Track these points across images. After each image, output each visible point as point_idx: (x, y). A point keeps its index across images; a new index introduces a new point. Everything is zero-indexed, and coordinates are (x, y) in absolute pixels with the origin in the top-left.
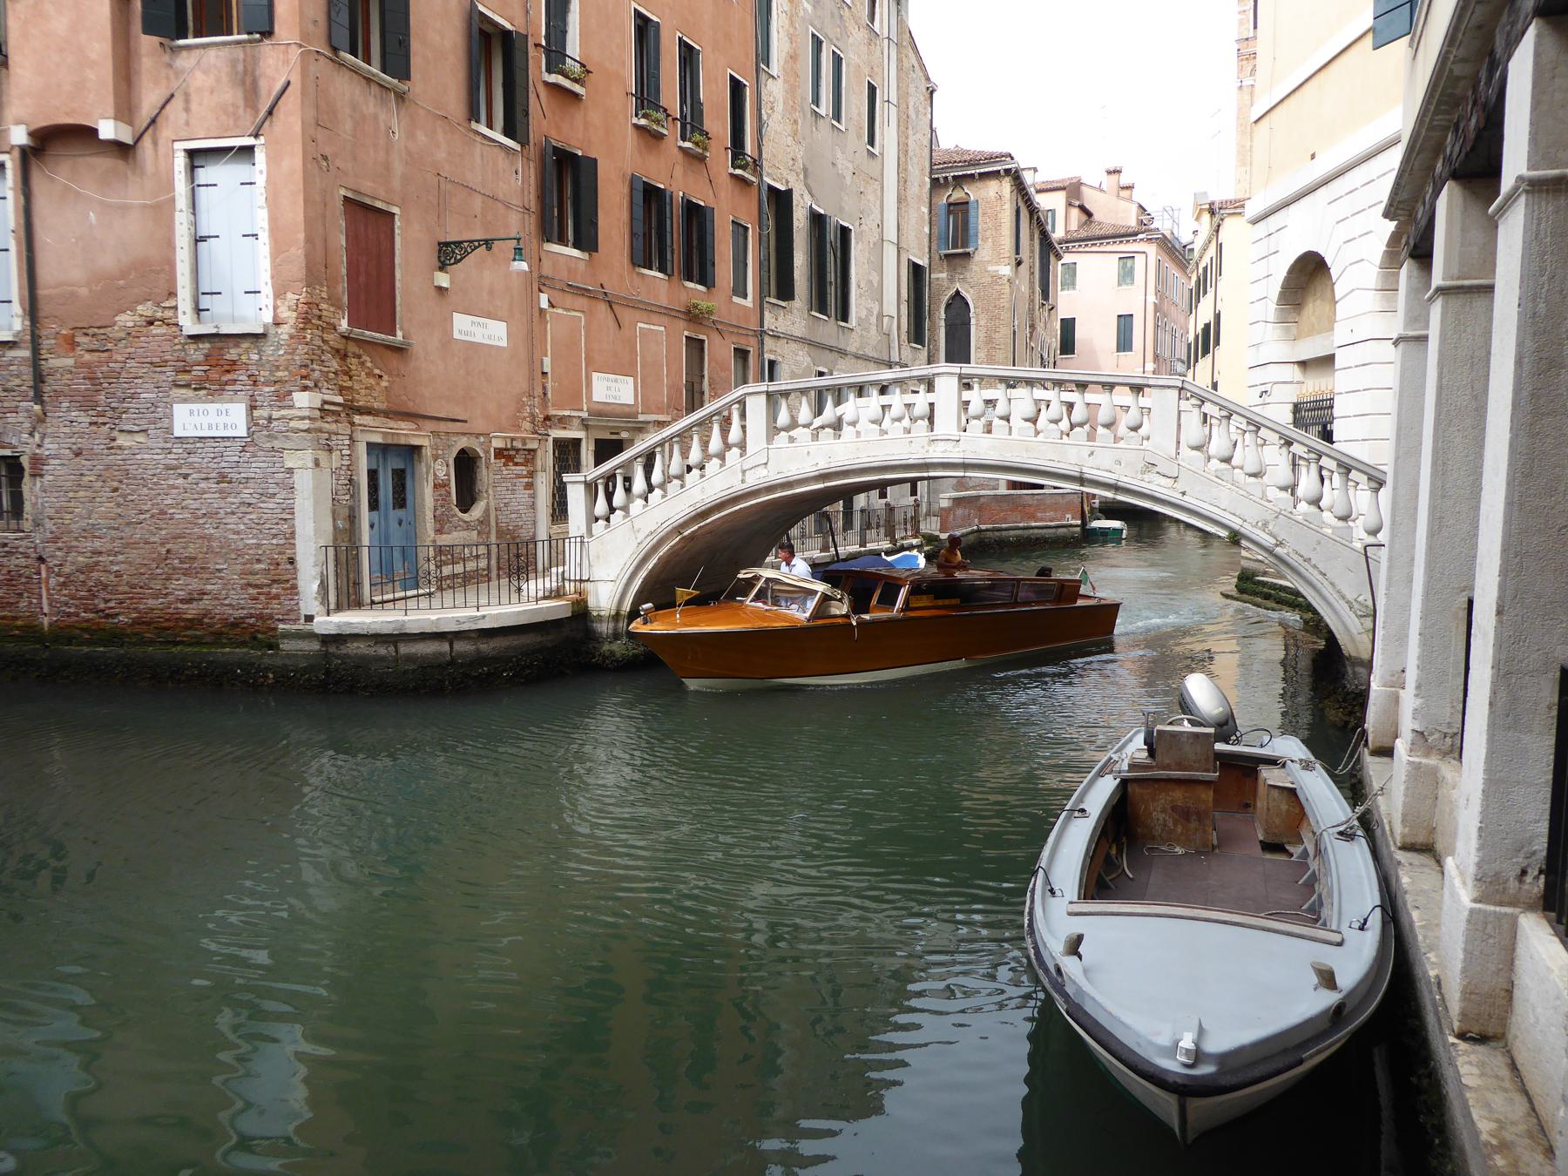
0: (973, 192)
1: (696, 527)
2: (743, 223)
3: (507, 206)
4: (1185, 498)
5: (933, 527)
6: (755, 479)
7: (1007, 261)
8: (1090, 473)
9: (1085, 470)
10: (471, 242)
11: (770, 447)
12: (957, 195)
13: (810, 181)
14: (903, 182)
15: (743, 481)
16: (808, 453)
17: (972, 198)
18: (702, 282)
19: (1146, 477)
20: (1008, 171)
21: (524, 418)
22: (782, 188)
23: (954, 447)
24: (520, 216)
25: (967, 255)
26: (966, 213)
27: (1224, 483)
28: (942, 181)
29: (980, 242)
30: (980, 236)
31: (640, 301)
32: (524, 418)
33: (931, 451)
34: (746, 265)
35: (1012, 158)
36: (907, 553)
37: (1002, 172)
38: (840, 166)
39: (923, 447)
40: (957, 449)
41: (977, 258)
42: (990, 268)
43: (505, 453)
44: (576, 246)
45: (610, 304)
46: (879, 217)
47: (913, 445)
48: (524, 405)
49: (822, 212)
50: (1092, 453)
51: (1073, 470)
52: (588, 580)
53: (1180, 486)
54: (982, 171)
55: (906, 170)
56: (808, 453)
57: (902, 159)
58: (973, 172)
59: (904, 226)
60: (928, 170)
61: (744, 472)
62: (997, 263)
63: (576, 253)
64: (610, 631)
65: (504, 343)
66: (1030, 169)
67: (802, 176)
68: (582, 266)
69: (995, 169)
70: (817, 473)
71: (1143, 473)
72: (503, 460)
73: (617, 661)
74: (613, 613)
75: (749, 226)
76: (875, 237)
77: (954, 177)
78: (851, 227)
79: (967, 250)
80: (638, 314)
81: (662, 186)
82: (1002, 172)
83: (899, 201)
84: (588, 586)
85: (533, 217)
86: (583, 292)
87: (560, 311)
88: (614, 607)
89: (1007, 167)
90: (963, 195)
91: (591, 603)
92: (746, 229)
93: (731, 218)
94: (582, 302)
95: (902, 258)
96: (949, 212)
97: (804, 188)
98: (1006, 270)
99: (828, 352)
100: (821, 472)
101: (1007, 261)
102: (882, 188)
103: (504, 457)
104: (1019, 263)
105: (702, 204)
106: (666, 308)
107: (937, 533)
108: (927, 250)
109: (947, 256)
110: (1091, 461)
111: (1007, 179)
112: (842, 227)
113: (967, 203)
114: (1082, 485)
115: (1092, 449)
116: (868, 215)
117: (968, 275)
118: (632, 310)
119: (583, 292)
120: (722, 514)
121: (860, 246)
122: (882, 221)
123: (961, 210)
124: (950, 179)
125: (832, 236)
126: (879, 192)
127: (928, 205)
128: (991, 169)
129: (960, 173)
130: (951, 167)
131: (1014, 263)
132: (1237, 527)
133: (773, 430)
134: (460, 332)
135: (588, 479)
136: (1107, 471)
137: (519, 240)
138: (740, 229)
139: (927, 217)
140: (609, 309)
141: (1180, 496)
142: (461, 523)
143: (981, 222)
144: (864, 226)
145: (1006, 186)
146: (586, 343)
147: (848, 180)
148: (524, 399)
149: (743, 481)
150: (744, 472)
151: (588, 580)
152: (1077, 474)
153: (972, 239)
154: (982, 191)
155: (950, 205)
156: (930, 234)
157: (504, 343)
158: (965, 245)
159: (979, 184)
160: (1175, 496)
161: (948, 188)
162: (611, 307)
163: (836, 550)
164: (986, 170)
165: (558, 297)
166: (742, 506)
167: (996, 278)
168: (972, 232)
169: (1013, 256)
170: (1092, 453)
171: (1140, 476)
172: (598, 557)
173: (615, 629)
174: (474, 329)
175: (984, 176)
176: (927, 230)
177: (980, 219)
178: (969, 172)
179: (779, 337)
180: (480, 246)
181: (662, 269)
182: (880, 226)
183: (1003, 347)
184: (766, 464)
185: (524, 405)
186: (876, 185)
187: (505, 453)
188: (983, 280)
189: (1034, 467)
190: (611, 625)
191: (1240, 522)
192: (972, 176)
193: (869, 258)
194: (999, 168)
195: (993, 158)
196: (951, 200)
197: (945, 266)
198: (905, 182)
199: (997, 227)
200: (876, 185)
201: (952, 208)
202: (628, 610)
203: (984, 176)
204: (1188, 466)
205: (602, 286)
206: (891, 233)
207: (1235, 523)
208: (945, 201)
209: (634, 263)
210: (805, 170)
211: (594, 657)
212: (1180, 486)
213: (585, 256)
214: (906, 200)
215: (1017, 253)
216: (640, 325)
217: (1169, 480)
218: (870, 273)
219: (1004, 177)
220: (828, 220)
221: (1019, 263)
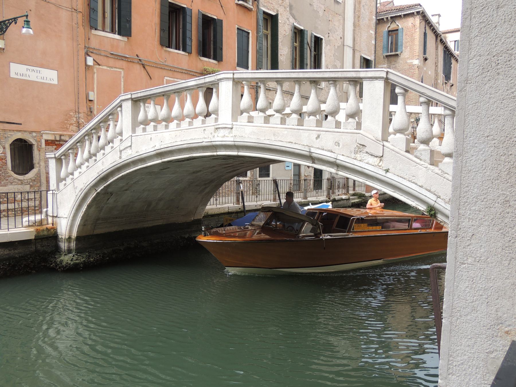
0: (400, 24)
1: (103, 187)
2: (245, 30)
3: (59, 6)
4: (389, 175)
5: (363, 190)
6: (128, 155)
7: (417, 57)
8: (317, 152)
9: (313, 150)
10: (9, 20)
11: (133, 135)
12: (393, 26)
13: (294, 12)
14: (357, 17)
15: (120, 158)
16: (151, 139)
17: (400, 27)
18: (215, 59)
19: (358, 156)
20: (418, 13)
21: (72, 124)
22: (273, 13)
23: (229, 133)
24: (70, 13)
25: (397, 55)
26: (397, 35)
27: (422, 163)
28: (385, 20)
29: (403, 48)
30: (404, 46)
31: (167, 65)
32: (72, 124)
33: (216, 136)
34: (248, 52)
35: (421, 6)
36: (325, 204)
37: (415, 13)
38: (315, 6)
39: (211, 133)
40: (231, 135)
41: (402, 56)
42: (409, 61)
43: (57, 143)
44: (119, 34)
45: (144, 66)
46: (342, 33)
47: (206, 132)
48: (71, 117)
49: (302, 28)
50: (318, 136)
51: (303, 150)
52: (57, 217)
53: (385, 164)
54: (405, 13)
55: (359, 11)
56: (151, 139)
57: (357, 6)
58: (400, 14)
59: (358, 39)
60: (374, 13)
61: (121, 151)
62: (412, 59)
63: (117, 36)
64: (66, 248)
65: (55, 82)
66: (436, 15)
67: (288, 9)
68: (122, 44)
69: (412, 12)
70: (154, 152)
71: (356, 153)
72: (55, 147)
73: (63, 267)
74: (67, 237)
75: (250, 31)
76: (340, 42)
77: (391, 17)
78: (322, 37)
79: (397, 53)
80: (164, 72)
81: (185, 6)
82: (415, 13)
83: (355, 25)
84: (58, 219)
85: (80, 16)
86: (123, 58)
87: (105, 68)
88: (67, 234)
89: (418, 10)
90: (395, 26)
91: (59, 231)
92: (248, 33)
93: (237, 26)
94: (124, 64)
95: (356, 55)
96: (389, 35)
97: (289, 15)
98: (416, 62)
99: (305, 99)
100: (157, 151)
101: (417, 57)
102: (344, 19)
103: (56, 145)
104: (426, 59)
105: (215, 18)
106: (186, 70)
107: (364, 193)
108: (373, 52)
109: (387, 56)
110: (317, 143)
111: (418, 16)
112: (315, 36)
113: (397, 30)
114: (313, 162)
115: (319, 133)
116: (334, 32)
117: (397, 65)
118: (160, 70)
119: (123, 58)
120: (114, 179)
121: (328, 47)
122: (344, 36)
123: (393, 33)
124: (389, 18)
125: (309, 39)
126: (342, 21)
127: (374, 30)
128: (409, 12)
129: (394, 15)
130: (390, 13)
131: (422, 59)
132: (432, 203)
133: (135, 124)
134: (17, 74)
135: (57, 155)
136: (329, 151)
137: (27, 16)
138: (243, 35)
139: (374, 36)
140: (143, 69)
141: (383, 173)
142: (15, 180)
143: (404, 39)
144: (331, 38)
145: (417, 20)
146: (124, 84)
147: (321, 13)
148: (72, 114)
149: (120, 158)
150: (121, 151)
151: (57, 217)
152: (307, 154)
153: (399, 47)
154: (405, 23)
155: (389, 31)
156: (375, 44)
157: (55, 82)
158: (396, 50)
159: (404, 20)
160: (380, 173)
161: (388, 23)
162: (144, 67)
163: (280, 201)
164: (407, 13)
165: (99, 59)
166: (123, 174)
167: (412, 66)
168: (399, 44)
169: (422, 55)
170: (318, 136)
171: (353, 156)
172: (61, 203)
173: (69, 247)
174: (28, 73)
175: (406, 16)
176: (373, 42)
177: (404, 37)
178: (398, 14)
179: (270, 90)
180: (12, 21)
181: (184, 50)
182: (342, 38)
183: (414, 100)
184: (131, 146)
185: (71, 117)
186: (340, 18)
187: (57, 143)
188: (405, 68)
189: (278, 148)
190: (66, 244)
191: (434, 198)
192: (400, 16)
193: (335, 54)
194: (414, 11)
195: (410, 7)
196: (390, 29)
197: (386, 62)
198: (359, 17)
199: (413, 40)
200: (340, 18)
201: (390, 33)
202: (75, 236)
203: (406, 16)
204: (392, 147)
205: (138, 56)
206: (349, 41)
207: (431, 199)
208: (386, 30)
209: (162, 44)
210: (291, 7)
211: (52, 264)
212: (385, 164)
213: (125, 39)
214: (359, 26)
215: (425, 52)
216: (166, 78)
217: (376, 159)
218: (335, 61)
219: (416, 15)
220: (305, 32)
221: (426, 59)
